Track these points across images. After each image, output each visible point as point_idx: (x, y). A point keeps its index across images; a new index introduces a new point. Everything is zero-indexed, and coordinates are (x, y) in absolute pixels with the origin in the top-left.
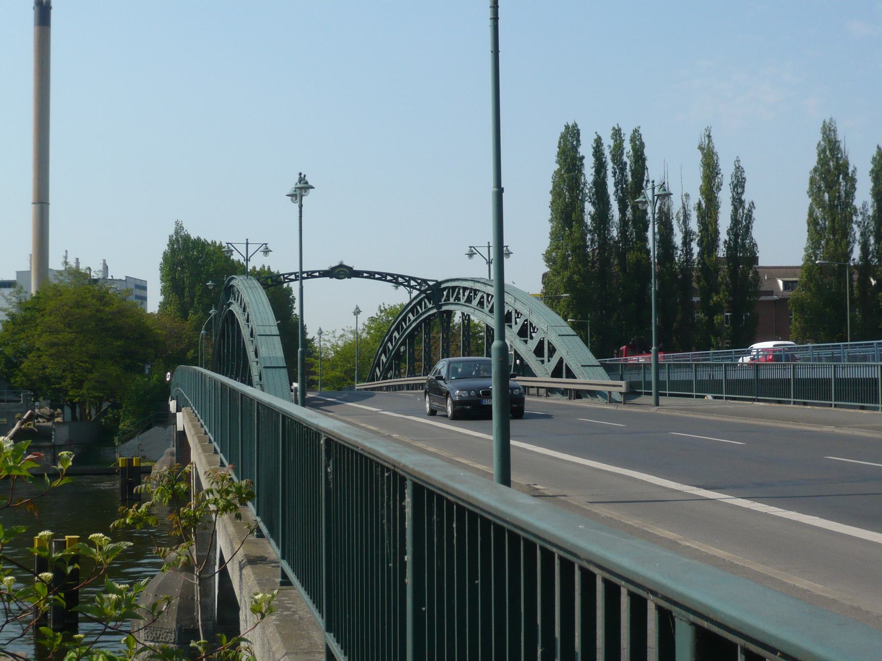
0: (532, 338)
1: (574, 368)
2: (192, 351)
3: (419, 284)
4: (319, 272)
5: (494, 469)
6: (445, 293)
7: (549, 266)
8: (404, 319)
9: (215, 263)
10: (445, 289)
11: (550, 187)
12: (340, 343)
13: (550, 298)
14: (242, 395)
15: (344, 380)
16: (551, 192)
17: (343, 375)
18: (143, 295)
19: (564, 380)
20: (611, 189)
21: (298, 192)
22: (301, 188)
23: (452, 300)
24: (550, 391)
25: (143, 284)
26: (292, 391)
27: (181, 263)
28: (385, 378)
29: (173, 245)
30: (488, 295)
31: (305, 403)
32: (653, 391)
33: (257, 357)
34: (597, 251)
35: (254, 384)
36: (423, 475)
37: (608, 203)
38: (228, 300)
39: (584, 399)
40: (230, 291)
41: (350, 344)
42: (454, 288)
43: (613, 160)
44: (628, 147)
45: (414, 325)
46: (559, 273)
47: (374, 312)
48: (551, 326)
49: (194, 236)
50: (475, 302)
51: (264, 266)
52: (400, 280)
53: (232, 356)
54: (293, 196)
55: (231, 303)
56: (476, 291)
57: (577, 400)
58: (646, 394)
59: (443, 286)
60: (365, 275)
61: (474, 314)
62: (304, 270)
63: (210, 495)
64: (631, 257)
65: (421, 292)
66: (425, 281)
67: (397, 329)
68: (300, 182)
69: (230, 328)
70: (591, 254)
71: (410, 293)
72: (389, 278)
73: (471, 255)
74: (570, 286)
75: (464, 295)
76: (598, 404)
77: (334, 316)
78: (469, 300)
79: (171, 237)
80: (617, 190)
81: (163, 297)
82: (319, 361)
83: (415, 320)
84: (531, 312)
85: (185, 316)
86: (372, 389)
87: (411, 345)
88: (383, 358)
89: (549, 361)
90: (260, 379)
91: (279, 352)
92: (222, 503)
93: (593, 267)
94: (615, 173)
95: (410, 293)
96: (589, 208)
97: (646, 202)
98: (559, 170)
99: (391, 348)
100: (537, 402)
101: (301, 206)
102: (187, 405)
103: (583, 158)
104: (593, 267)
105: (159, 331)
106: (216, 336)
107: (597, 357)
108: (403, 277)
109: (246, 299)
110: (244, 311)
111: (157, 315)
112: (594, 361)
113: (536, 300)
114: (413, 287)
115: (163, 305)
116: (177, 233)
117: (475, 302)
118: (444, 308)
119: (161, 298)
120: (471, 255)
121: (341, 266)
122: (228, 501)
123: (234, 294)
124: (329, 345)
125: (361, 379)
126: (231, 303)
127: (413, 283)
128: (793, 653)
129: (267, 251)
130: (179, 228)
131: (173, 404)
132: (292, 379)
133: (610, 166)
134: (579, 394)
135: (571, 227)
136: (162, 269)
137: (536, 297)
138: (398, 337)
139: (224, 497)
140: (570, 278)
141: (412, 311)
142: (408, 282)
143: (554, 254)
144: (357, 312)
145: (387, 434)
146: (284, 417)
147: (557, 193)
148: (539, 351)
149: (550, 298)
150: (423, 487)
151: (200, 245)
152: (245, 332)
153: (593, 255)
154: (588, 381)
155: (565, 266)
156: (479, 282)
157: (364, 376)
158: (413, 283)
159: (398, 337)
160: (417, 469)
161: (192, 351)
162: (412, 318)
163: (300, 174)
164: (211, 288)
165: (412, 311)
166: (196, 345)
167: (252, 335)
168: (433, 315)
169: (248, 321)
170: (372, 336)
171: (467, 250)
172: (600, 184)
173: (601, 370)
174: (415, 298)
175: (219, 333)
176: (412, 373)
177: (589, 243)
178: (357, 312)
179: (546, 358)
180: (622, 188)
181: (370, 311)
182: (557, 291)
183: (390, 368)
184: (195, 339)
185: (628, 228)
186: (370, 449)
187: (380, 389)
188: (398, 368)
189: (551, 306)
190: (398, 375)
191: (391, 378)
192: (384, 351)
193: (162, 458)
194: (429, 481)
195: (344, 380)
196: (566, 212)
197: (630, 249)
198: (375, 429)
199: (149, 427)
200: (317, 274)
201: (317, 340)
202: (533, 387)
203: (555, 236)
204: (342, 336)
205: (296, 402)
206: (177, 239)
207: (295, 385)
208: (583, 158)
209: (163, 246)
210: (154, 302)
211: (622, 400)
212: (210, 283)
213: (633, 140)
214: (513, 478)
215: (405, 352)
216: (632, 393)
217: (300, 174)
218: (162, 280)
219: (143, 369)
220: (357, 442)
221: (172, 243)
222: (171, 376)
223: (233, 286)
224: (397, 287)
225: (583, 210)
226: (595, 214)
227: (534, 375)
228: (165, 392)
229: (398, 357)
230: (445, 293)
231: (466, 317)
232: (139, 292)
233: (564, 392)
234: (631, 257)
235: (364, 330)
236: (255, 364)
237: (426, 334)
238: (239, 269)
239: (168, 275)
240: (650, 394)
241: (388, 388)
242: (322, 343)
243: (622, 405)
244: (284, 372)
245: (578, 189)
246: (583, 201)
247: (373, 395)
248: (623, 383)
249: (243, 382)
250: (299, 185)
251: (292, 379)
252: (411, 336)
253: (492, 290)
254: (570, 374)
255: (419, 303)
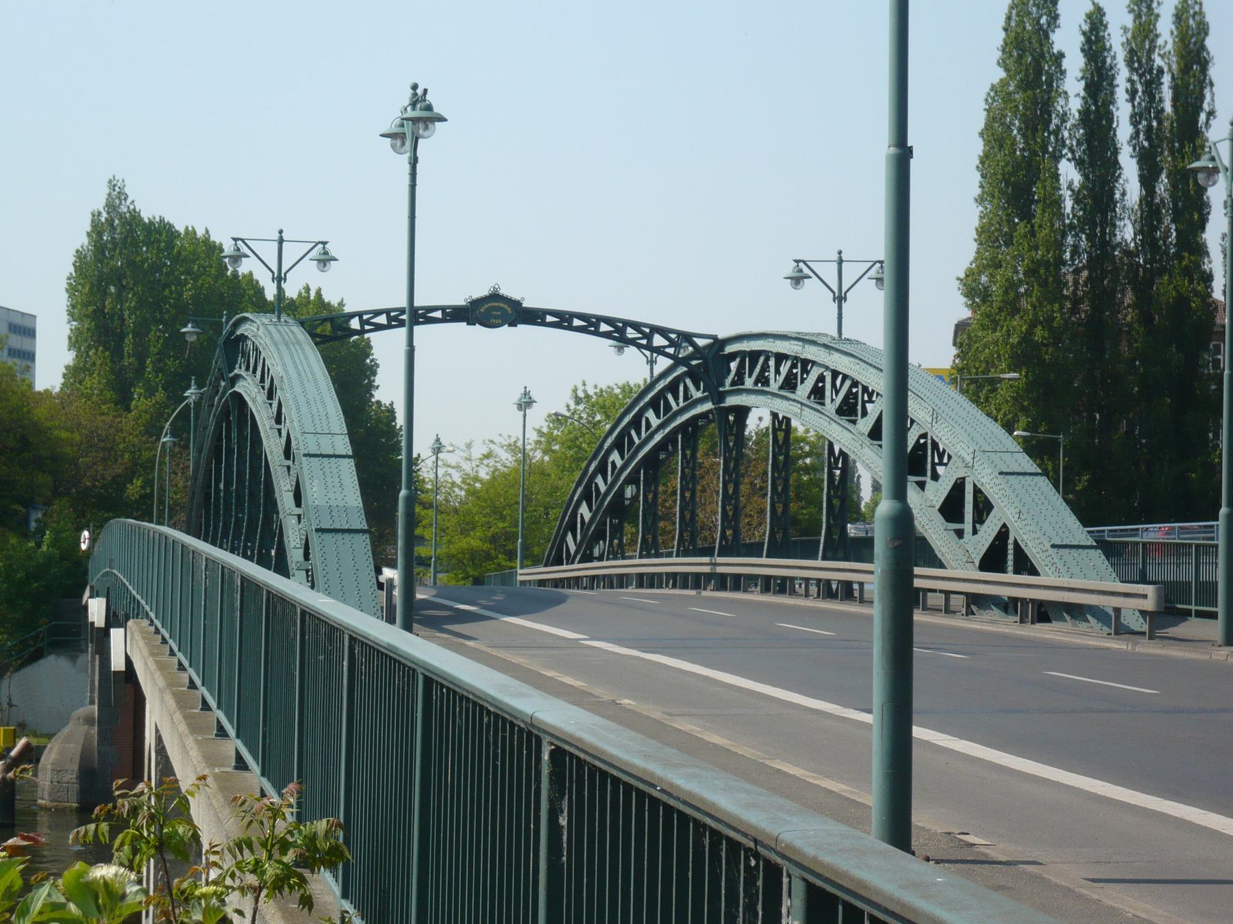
0: (935, 477)
1: (1034, 551)
2: (138, 483)
3: (672, 343)
4: (443, 309)
5: (871, 796)
6: (734, 365)
7: (973, 307)
8: (636, 423)
9: (195, 280)
10: (732, 356)
11: (979, 120)
12: (484, 474)
13: (973, 381)
14: (303, 613)
15: (488, 557)
16: (981, 134)
17: (486, 546)
18: (26, 347)
19: (1010, 577)
20: (1123, 131)
21: (408, 129)
22: (415, 121)
23: (749, 382)
24: (977, 602)
25: (27, 323)
26: (380, 586)
27: (117, 277)
28: (587, 558)
29: (100, 234)
30: (835, 374)
31: (413, 616)
32: (1220, 609)
33: (298, 504)
34: (1085, 274)
35: (292, 566)
36: (845, 875)
37: (1113, 165)
38: (231, 369)
39: (1055, 625)
40: (236, 347)
41: (505, 476)
42: (754, 356)
43: (1129, 63)
44: (1165, 28)
45: (658, 437)
46: (995, 325)
47: (561, 403)
48: (977, 445)
49: (148, 213)
50: (804, 390)
51: (307, 289)
52: (631, 333)
53: (238, 499)
54: (395, 137)
55: (238, 377)
56: (806, 364)
57: (1038, 626)
58: (1200, 614)
59: (729, 349)
60: (549, 319)
61: (799, 416)
62: (416, 304)
63: (246, 851)
64: (1166, 288)
65: (678, 361)
66: (687, 337)
67: (618, 445)
68: (413, 105)
69: (234, 435)
70: (1070, 278)
71: (652, 362)
72: (604, 327)
73: (797, 280)
74: (1025, 355)
75: (778, 372)
76: (1090, 636)
77: (475, 412)
78: (790, 384)
79: (96, 216)
80: (1137, 133)
81: (73, 354)
82: (431, 512)
83: (661, 426)
84: (935, 416)
85: (123, 400)
86: (557, 583)
87: (652, 481)
88: (584, 510)
89: (975, 532)
90: (307, 556)
91: (353, 498)
92: (271, 870)
93: (1074, 310)
94: (1132, 93)
95: (652, 362)
96: (1069, 173)
97: (1215, 170)
98: (1004, 83)
99: (603, 488)
100: (942, 627)
101: (414, 162)
102: (138, 613)
103: (1061, 55)
104: (1074, 310)
105: (64, 435)
106: (200, 451)
107: (1086, 520)
108: (636, 326)
109: (276, 369)
110: (270, 396)
111: (59, 396)
112: (1079, 533)
113: (939, 384)
114: (660, 351)
115: (74, 374)
116: (111, 206)
117: (804, 390)
118: (731, 401)
119: (69, 357)
120: (797, 280)
121: (495, 296)
122: (286, 865)
123: (246, 355)
124: (457, 477)
125: (532, 559)
126: (238, 377)
127: (658, 341)
128: (911, 917)
129: (325, 260)
130: (117, 195)
131: (96, 610)
132: (381, 561)
133: (1122, 76)
134: (1043, 612)
135: (1027, 216)
136: (71, 290)
137: (938, 374)
138: (619, 463)
139: (276, 856)
140: (1027, 338)
141: (654, 404)
142: (649, 337)
143: (984, 279)
144: (526, 403)
145: (607, 697)
146: (428, 681)
147: (995, 135)
148: (951, 509)
149: (973, 378)
150: (836, 898)
151: (160, 235)
152: (272, 446)
153: (1076, 283)
154: (1065, 581)
155: (1012, 307)
156: (814, 343)
157: (536, 550)
158: (658, 341)
159: (619, 463)
160: (827, 859)
161: (138, 483)
162: (655, 422)
163: (415, 87)
164: (192, 339)
165: (654, 404)
166: (149, 466)
167: (288, 452)
168: (704, 415)
169: (278, 419)
170: (555, 461)
171: (789, 269)
172: (1097, 121)
173: (1097, 556)
174: (663, 375)
175: (207, 444)
176: (650, 548)
177: (1067, 255)
178: (526, 403)
179: (968, 526)
180: (1150, 127)
181: (554, 399)
182: (989, 364)
183: (599, 535)
184: (147, 455)
185: (1160, 221)
186: (690, 794)
187: (576, 582)
188: (617, 531)
189: (975, 400)
190: (617, 553)
191: (600, 559)
192: (587, 497)
193: (66, 731)
194: (862, 892)
195: (488, 557)
196: (1014, 182)
197: (1162, 271)
198: (577, 683)
199: (37, 656)
200: (438, 314)
201: (430, 462)
202: (934, 591)
203: (987, 235)
204: (488, 456)
205: (391, 620)
206: (110, 222)
207: (388, 573)
208: (1061, 55)
209: (79, 238)
210: (52, 364)
211: (1146, 628)
212: (189, 328)
213: (1179, 18)
214: (919, 818)
215: (635, 498)
216: (1169, 612)
217: (415, 87)
218: (71, 314)
219: (26, 520)
220: (652, 774)
221: (97, 229)
222: (93, 540)
223: (243, 338)
224: (620, 349)
225: (1056, 177)
226: (1083, 187)
227: (941, 566)
228: (73, 576)
229: (619, 509)
230: (734, 365)
231: (781, 425)
232: (16, 341)
233: (1009, 606)
234: (1166, 288)
235: (538, 442)
236: (294, 521)
237: (696, 470)
238: (245, 296)
239: (86, 305)
240: (1213, 616)
241: (594, 582)
242: (441, 472)
243: (1145, 640)
244: (363, 544)
245: (1046, 128)
246: (1056, 158)
247: (561, 600)
248: (1149, 590)
249: (263, 562)
250: (410, 113)
251: (381, 561)
252: (654, 465)
253: (879, 382)
254: (1024, 565)
255: (673, 388)
